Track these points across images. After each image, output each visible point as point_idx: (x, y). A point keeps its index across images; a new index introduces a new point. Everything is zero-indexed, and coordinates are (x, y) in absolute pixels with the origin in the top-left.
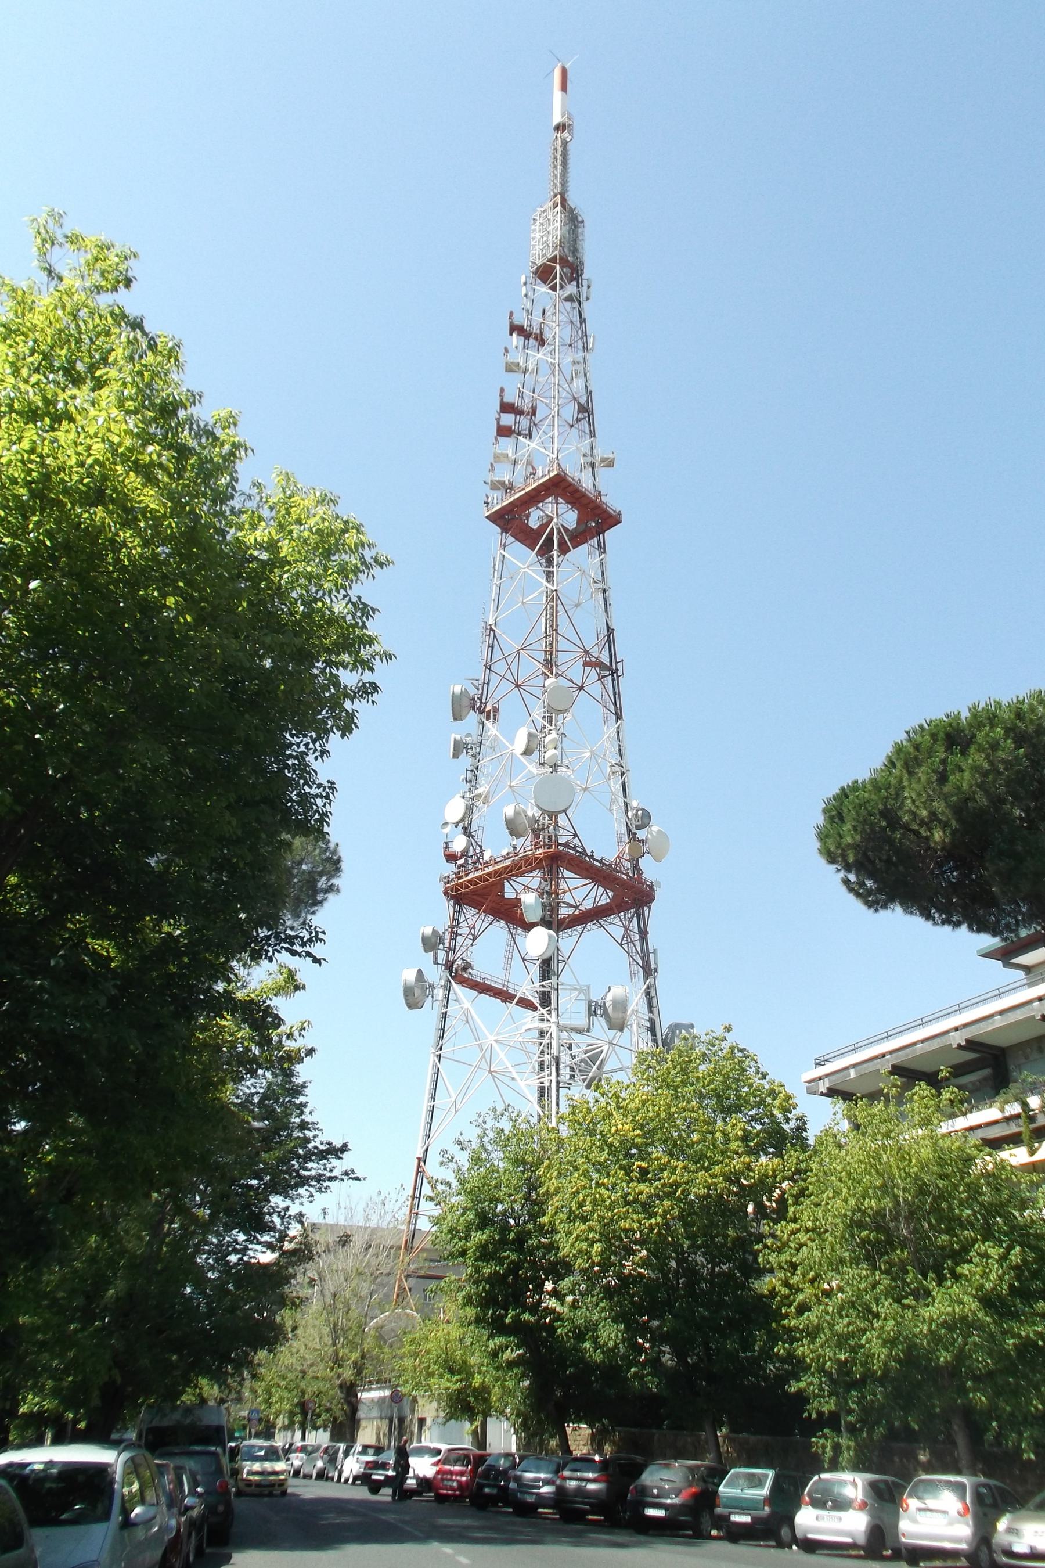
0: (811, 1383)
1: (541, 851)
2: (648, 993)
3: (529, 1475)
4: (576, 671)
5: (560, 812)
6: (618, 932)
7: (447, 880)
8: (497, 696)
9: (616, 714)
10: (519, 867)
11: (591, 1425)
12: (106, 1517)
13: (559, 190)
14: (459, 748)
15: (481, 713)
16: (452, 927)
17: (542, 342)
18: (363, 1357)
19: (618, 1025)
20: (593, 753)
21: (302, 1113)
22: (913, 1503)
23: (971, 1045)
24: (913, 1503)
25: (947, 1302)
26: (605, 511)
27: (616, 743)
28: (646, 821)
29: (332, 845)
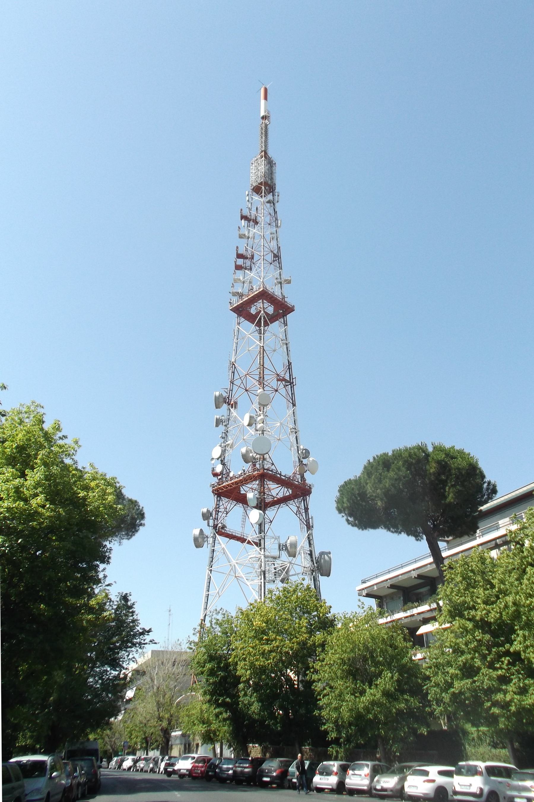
0: (329, 726)
1: (256, 472)
2: (309, 538)
3: (225, 766)
4: (274, 383)
5: (265, 454)
6: (295, 509)
7: (213, 486)
8: (236, 397)
9: (293, 404)
10: (247, 480)
11: (260, 745)
12: (45, 775)
13: (263, 149)
14: (218, 422)
15: (229, 405)
16: (216, 508)
17: (256, 222)
18: (171, 716)
19: (293, 555)
20: (281, 424)
21: (133, 615)
22: (351, 772)
23: (420, 577)
24: (351, 772)
25: (372, 694)
26: (287, 306)
27: (293, 418)
28: (307, 455)
29: (141, 508)
